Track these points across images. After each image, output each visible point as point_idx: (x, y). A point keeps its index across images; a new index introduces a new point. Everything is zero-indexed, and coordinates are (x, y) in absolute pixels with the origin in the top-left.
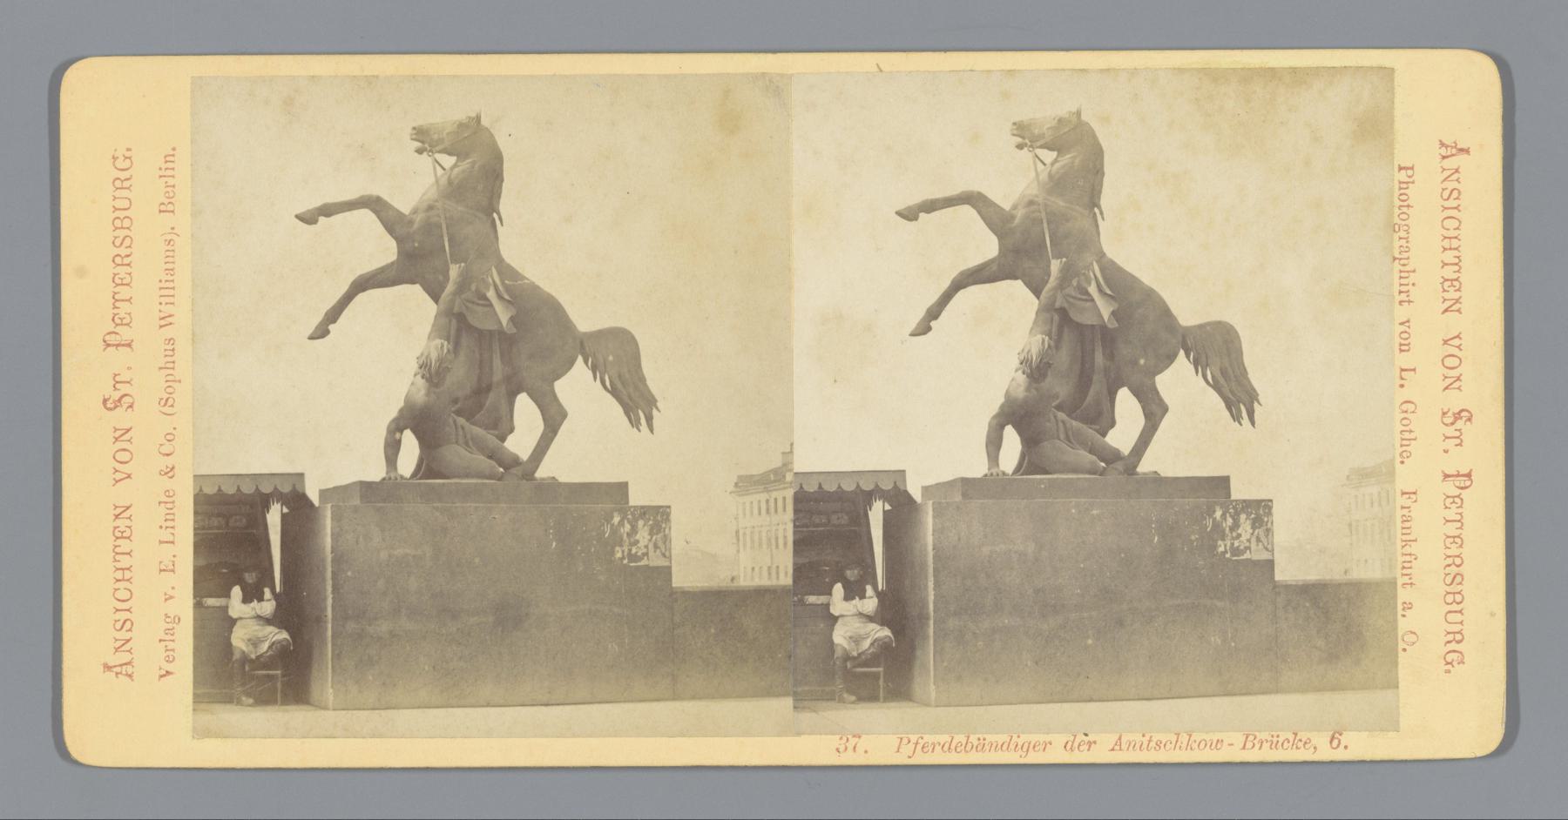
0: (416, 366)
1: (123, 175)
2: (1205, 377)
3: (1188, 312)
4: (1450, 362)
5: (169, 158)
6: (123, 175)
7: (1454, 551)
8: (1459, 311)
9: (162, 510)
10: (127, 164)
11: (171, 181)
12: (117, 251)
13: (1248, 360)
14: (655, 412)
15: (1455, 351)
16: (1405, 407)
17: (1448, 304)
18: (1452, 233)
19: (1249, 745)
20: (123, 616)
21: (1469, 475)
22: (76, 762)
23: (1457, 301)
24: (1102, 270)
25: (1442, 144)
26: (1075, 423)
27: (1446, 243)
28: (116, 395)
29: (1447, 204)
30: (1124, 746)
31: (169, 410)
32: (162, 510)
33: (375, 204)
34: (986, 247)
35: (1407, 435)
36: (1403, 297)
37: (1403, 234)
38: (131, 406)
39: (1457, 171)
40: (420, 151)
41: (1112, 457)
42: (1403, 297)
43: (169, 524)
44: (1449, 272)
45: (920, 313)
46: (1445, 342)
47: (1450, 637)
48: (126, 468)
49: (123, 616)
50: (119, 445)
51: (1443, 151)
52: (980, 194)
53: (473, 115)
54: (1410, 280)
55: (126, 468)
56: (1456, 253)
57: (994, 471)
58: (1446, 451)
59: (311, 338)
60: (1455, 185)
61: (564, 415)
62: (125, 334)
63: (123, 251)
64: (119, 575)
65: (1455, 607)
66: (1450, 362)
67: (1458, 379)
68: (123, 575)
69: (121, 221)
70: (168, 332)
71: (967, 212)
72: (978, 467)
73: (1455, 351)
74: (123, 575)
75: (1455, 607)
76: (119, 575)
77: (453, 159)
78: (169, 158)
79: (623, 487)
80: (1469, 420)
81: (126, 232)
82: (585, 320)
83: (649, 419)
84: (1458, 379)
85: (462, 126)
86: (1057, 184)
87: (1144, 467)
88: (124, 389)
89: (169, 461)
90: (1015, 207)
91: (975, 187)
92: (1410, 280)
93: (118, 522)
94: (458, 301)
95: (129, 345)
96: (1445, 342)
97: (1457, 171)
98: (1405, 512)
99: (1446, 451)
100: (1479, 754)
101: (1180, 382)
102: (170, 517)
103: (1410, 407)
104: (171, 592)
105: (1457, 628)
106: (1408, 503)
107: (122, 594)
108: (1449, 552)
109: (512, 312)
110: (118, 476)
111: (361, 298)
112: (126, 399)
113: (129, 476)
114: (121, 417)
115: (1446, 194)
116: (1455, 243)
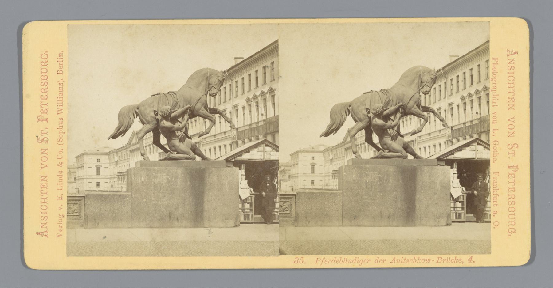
1: (512, 226)
4: (511, 127)
5: (61, 55)
6: (512, 226)
7: (512, 193)
8: (514, 109)
9: (58, 178)
10: (46, 57)
11: (61, 63)
12: (514, 200)
15: (43, 163)
16: (495, 143)
17: (45, 179)
18: (511, 82)
19: (439, 261)
20: (44, 215)
21: (517, 167)
22: (30, 268)
23: (513, 106)
25: (508, 51)
27: (509, 85)
28: (514, 149)
29: (509, 71)
30: (396, 262)
31: (59, 143)
32: (58, 178)
35: (495, 153)
36: (494, 104)
37: (494, 82)
38: (47, 142)
39: (513, 60)
42: (494, 104)
43: (61, 183)
44: (510, 95)
46: (509, 120)
47: (510, 223)
48: (510, 123)
49: (44, 215)
50: (512, 131)
51: (46, 234)
54: (497, 98)
55: (510, 123)
56: (513, 89)
58: (47, 128)
60: (43, 222)
62: (510, 171)
63: (512, 200)
64: (43, 201)
65: (512, 213)
66: (511, 127)
67: (514, 133)
68: (44, 201)
69: (45, 78)
70: (60, 116)
73: (512, 123)
74: (44, 201)
75: (512, 213)
76: (43, 201)
78: (61, 55)
80: (517, 147)
81: (511, 206)
84: (514, 133)
88: (511, 151)
89: (61, 161)
92: (497, 98)
93: (513, 103)
95: (509, 167)
96: (509, 120)
97: (513, 60)
98: (495, 179)
99: (47, 128)
100: (33, 22)
102: (61, 180)
103: (496, 143)
104: (61, 207)
105: (513, 220)
106: (496, 176)
107: (511, 78)
108: (510, 194)
110: (512, 120)
112: (46, 139)
113: (46, 166)
114: (43, 146)
115: (509, 68)
116: (512, 85)
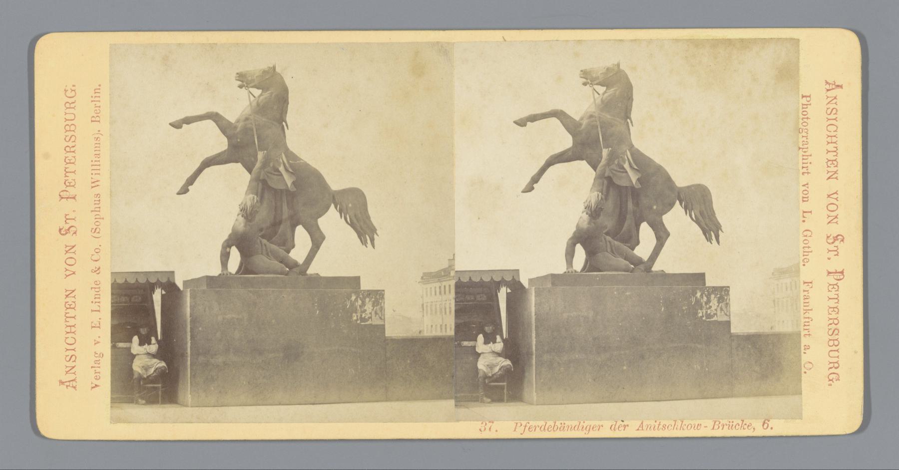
0: (239, 210)
1: (71, 100)
2: (691, 216)
3: (681, 179)
4: (832, 207)
5: (97, 91)
6: (71, 100)
7: (834, 316)
8: (836, 178)
9: (93, 292)
10: (73, 94)
11: (98, 104)
12: (67, 144)
13: (715, 206)
14: (375, 236)
15: (834, 201)
16: (805, 233)
17: (830, 174)
18: (833, 134)
19: (716, 427)
20: (70, 353)
21: (842, 273)
22: (43, 437)
23: (835, 172)
24: (632, 155)
25: (827, 83)
26: (616, 243)
27: (829, 139)
28: (67, 227)
29: (829, 117)
30: (645, 428)
31: (97, 235)
32: (93, 292)
33: (215, 117)
34: (565, 142)
35: (807, 249)
36: (805, 170)
37: (804, 134)
38: (75, 233)
39: (835, 98)
40: (241, 87)
41: (637, 262)
42: (805, 170)
43: (97, 300)
44: (831, 156)
45: (528, 180)
46: (829, 196)
47: (832, 365)
48: (72, 268)
49: (70, 353)
50: (68, 255)
51: (828, 87)
52: (562, 111)
53: (271, 66)
54: (809, 161)
55: (72, 268)
56: (835, 145)
57: (570, 270)
58: (829, 259)
59: (178, 194)
60: (834, 106)
61: (323, 238)
62: (72, 191)
63: (71, 144)
64: (68, 329)
65: (834, 348)
66: (832, 207)
67: (836, 217)
68: (71, 329)
69: (70, 127)
70: (96, 190)
71: (555, 121)
72: (561, 268)
73: (834, 201)
74: (71, 329)
75: (834, 348)
76: (68, 329)
77: (260, 91)
78: (97, 91)
79: (357, 279)
80: (842, 240)
81: (72, 133)
82: (335, 184)
83: (372, 240)
84: (836, 217)
85: (265, 72)
86: (606, 105)
87: (656, 267)
88: (71, 223)
89: (97, 264)
90: (582, 119)
91: (559, 107)
92: (809, 161)
93: (68, 299)
94: (262, 173)
95: (74, 198)
96: (829, 196)
97: (835, 98)
98: (806, 293)
99: (829, 259)
100: (848, 432)
101: (676, 219)
102: (97, 297)
103: (808, 233)
104: (98, 339)
105: (835, 360)
106: (807, 288)
107: (70, 341)
108: (831, 317)
109: (294, 179)
110: (68, 273)
111: (207, 171)
112: (72, 229)
113: (74, 273)
114: (69, 239)
115: (829, 111)
116: (834, 139)
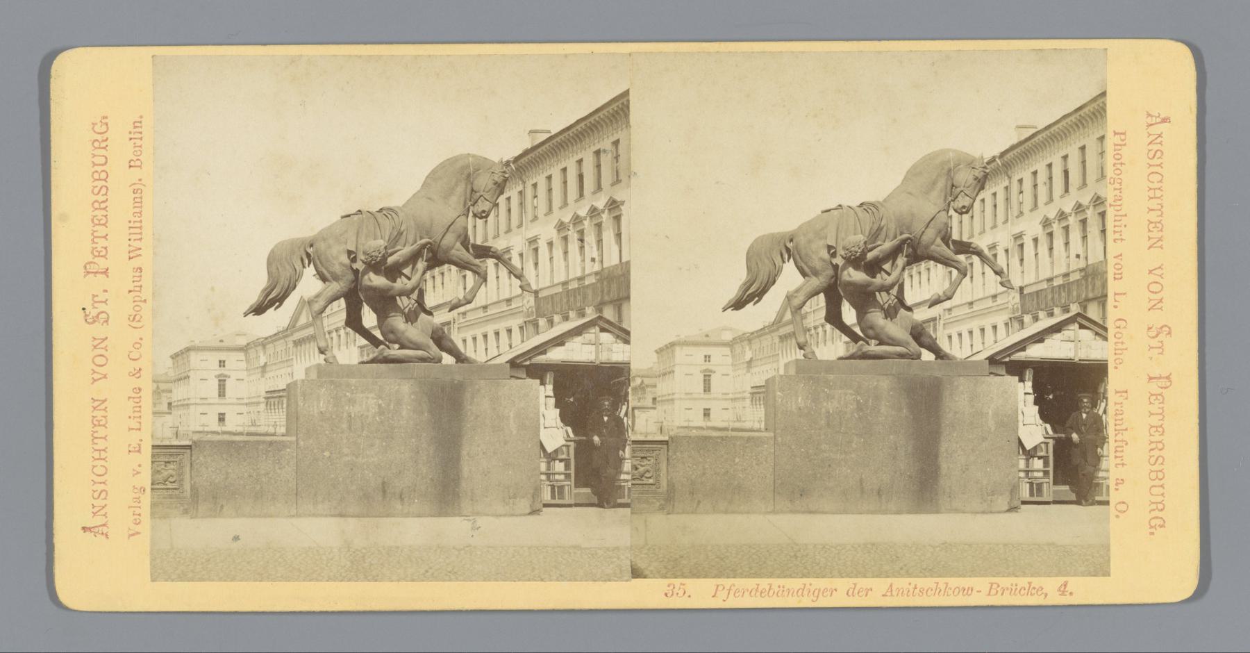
1: (1156, 513)
4: (1154, 288)
5: (137, 124)
6: (1156, 513)
7: (1157, 438)
8: (1161, 247)
9: (131, 403)
10: (104, 128)
11: (138, 142)
12: (1161, 453)
15: (97, 369)
16: (1118, 323)
17: (102, 407)
18: (1156, 185)
19: (993, 592)
20: (100, 487)
21: (1168, 378)
22: (67, 609)
23: (1160, 239)
25: (1149, 115)
27: (1151, 194)
28: (1161, 337)
29: (1151, 162)
30: (895, 593)
31: (134, 324)
32: (131, 403)
35: (1120, 346)
36: (1117, 236)
37: (1117, 186)
38: (107, 321)
39: (1160, 136)
42: (1117, 236)
43: (137, 414)
44: (1153, 216)
46: (1150, 272)
47: (1154, 506)
48: (1153, 278)
49: (100, 487)
50: (1158, 297)
51: (105, 530)
54: (1123, 222)
55: (1153, 278)
56: (1159, 201)
58: (105, 291)
60: (96, 503)
62: (1154, 387)
63: (1156, 453)
64: (96, 455)
65: (1157, 482)
66: (1154, 288)
67: (1161, 301)
68: (100, 455)
69: (101, 177)
70: (136, 263)
73: (1158, 279)
74: (100, 455)
75: (1157, 482)
76: (96, 455)
78: (137, 124)
80: (1169, 333)
81: (1154, 468)
84: (1161, 301)
88: (1154, 343)
89: (137, 365)
92: (1123, 222)
93: (1160, 234)
95: (1151, 378)
96: (1150, 272)
97: (1160, 136)
98: (1118, 407)
99: (105, 291)
100: (74, 50)
102: (138, 408)
103: (1122, 324)
104: (138, 469)
105: (1159, 499)
106: (1120, 400)
107: (1156, 178)
108: (1153, 439)
110: (1158, 272)
112: (103, 316)
113: (105, 377)
114: (98, 330)
115: (1151, 154)
116: (1158, 193)
